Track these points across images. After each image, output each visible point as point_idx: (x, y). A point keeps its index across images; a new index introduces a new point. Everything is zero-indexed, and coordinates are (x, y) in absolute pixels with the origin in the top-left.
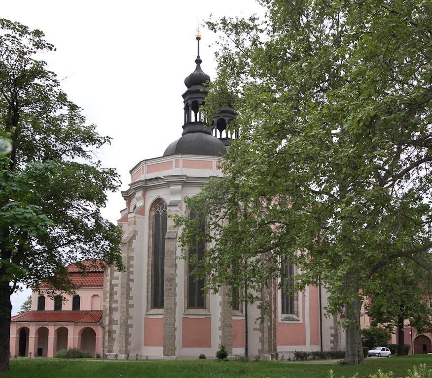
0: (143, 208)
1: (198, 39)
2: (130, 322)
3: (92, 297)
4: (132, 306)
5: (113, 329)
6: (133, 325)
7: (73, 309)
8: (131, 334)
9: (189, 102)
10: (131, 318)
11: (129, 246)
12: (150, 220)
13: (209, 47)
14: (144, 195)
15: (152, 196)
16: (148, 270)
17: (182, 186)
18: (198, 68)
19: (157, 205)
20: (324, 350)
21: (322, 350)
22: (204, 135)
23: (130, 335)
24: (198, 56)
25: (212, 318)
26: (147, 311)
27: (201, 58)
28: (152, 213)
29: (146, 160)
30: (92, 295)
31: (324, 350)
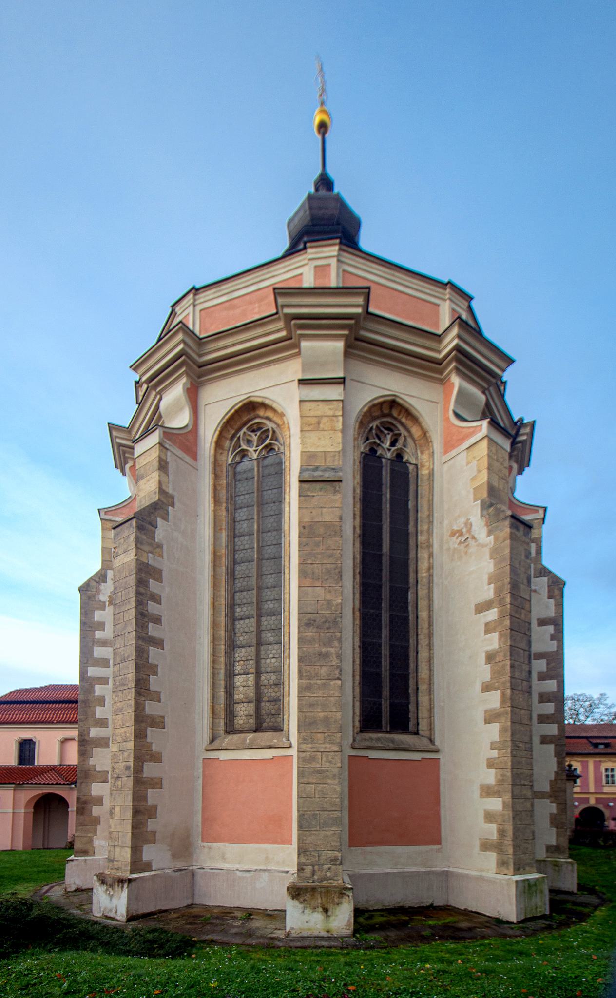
0: (194, 430)
2: (150, 770)
4: (158, 722)
5: (93, 793)
6: (481, 796)
8: (155, 807)
10: (156, 758)
19: (241, 433)
20: (236, 705)
21: (236, 703)
23: (152, 812)
25: (442, 761)
26: (212, 741)
27: (332, 173)
28: (224, 458)
29: (195, 291)
30: (60, 738)
31: (236, 705)
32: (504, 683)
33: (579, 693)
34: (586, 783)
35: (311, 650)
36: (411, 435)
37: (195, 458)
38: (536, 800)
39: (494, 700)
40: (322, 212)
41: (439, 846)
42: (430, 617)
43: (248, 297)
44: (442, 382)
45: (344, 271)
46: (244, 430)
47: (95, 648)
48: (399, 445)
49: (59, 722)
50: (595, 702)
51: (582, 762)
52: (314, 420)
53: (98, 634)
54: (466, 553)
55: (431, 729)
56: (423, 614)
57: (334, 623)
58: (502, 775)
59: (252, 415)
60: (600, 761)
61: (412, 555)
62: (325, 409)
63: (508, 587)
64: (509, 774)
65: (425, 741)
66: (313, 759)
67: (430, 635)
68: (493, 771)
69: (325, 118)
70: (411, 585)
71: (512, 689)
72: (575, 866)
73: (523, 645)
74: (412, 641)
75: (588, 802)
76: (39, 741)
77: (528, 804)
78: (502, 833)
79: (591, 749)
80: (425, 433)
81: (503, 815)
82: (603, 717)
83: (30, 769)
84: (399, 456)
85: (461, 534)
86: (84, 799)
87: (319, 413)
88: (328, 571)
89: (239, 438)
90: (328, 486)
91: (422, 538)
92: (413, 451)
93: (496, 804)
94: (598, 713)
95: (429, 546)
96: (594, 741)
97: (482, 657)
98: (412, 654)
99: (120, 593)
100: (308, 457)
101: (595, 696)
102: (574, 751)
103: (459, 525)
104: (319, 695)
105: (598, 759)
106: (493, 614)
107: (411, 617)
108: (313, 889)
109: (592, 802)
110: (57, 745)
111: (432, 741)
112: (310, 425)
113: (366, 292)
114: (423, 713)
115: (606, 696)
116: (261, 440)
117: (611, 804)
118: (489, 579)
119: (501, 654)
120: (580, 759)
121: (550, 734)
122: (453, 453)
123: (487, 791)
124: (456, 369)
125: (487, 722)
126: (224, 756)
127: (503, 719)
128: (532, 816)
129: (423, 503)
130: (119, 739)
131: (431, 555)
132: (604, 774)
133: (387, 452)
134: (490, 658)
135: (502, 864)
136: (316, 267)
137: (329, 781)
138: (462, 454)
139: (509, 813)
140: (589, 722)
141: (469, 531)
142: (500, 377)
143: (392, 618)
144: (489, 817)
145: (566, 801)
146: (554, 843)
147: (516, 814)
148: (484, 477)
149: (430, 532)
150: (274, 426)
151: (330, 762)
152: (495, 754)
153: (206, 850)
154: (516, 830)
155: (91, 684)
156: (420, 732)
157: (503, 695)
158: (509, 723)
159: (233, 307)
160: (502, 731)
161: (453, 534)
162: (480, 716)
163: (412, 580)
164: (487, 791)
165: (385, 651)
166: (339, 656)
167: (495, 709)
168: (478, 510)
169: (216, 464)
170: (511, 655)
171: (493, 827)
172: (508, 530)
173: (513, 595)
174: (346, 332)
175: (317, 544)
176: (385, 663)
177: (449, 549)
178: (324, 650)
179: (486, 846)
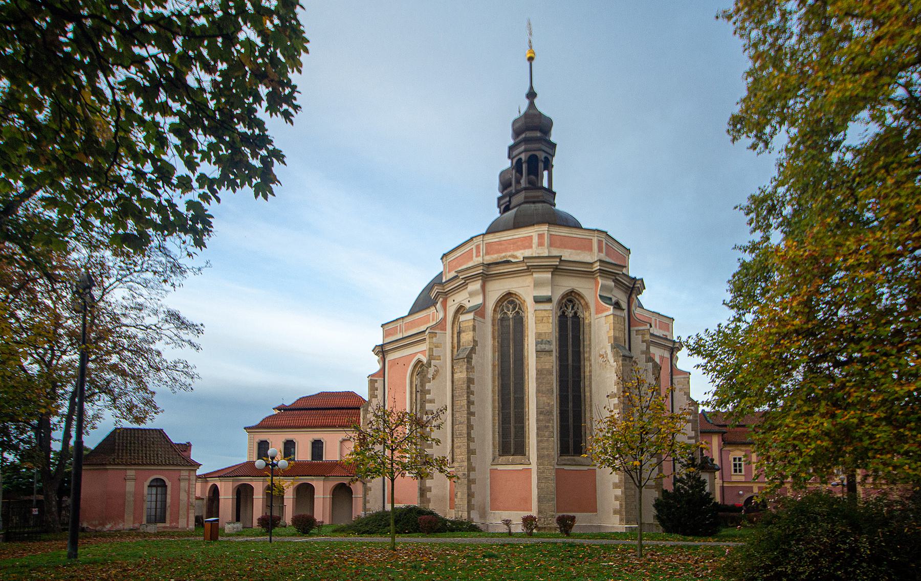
1: (531, 59)
5: (427, 485)
7: (312, 459)
11: (468, 362)
12: (493, 325)
14: (483, 287)
15: (497, 289)
16: (493, 401)
17: (552, 274)
18: (532, 105)
24: (531, 87)
26: (493, 460)
27: (536, 90)
30: (341, 439)
37: (484, 318)
42: (591, 396)
44: (595, 279)
48: (575, 308)
49: (340, 426)
53: (428, 397)
56: (588, 394)
57: (551, 413)
62: (545, 314)
66: (543, 472)
67: (591, 406)
69: (532, 55)
74: (583, 408)
75: (752, 491)
78: (621, 505)
80: (587, 304)
83: (318, 465)
84: (576, 313)
88: (548, 390)
90: (547, 353)
91: (586, 355)
93: (619, 492)
95: (590, 360)
98: (583, 415)
100: (538, 335)
104: (545, 444)
107: (582, 395)
108: (545, 528)
110: (338, 444)
112: (539, 321)
116: (514, 309)
120: (743, 448)
122: (599, 316)
126: (500, 468)
129: (587, 337)
130: (459, 461)
132: (732, 463)
133: (570, 313)
135: (621, 520)
141: (607, 357)
143: (574, 396)
148: (612, 333)
149: (590, 352)
154: (627, 504)
161: (600, 356)
163: (582, 377)
165: (571, 415)
166: (553, 427)
168: (610, 348)
169: (493, 320)
175: (543, 379)
176: (571, 421)
179: (615, 512)
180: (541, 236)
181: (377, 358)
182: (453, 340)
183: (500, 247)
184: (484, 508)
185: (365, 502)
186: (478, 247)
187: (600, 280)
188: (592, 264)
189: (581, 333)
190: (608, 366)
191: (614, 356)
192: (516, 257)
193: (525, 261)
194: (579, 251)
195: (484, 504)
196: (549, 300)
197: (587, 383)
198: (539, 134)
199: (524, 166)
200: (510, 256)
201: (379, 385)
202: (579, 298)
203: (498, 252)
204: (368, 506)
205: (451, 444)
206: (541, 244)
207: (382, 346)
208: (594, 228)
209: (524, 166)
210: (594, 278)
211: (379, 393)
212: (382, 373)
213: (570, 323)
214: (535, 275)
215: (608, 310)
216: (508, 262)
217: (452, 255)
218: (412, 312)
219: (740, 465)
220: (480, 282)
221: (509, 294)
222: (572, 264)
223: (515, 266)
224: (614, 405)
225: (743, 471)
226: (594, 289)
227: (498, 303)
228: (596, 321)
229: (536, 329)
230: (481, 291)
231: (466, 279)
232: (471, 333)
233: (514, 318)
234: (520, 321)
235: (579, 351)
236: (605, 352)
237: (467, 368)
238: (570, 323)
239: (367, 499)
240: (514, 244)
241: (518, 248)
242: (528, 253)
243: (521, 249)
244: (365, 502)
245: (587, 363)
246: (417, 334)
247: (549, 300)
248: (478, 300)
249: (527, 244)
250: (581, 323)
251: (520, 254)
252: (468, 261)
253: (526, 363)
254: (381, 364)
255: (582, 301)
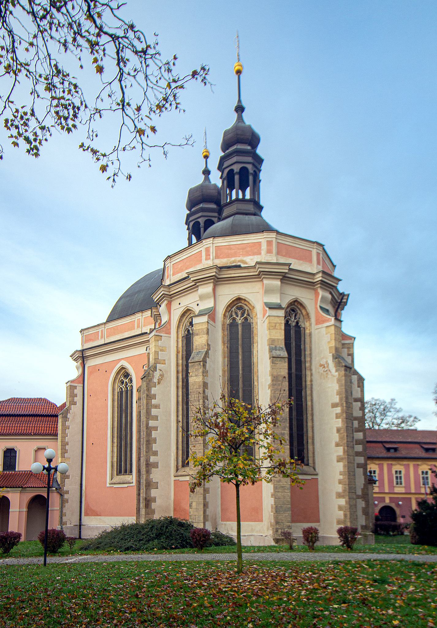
1: (239, 72)
3: (36, 451)
5: (152, 495)
6: (337, 498)
7: (4, 470)
9: (233, 167)
13: (184, 111)
14: (214, 290)
18: (240, 119)
19: (233, 309)
22: (253, 217)
24: (239, 101)
25: (319, 479)
27: (244, 104)
30: (35, 448)
32: (344, 444)
33: (376, 398)
34: (382, 486)
35: (278, 432)
36: (302, 313)
38: (357, 500)
39: (340, 451)
40: (242, 137)
41: (319, 524)
42: (312, 406)
43: (237, 246)
44: (315, 290)
45: (278, 242)
46: (235, 307)
47: (152, 409)
48: (297, 317)
49: (35, 435)
50: (388, 406)
51: (379, 464)
52: (274, 325)
53: (154, 402)
54: (327, 377)
55: (314, 463)
56: (309, 403)
58: (345, 488)
59: (239, 302)
60: (391, 464)
61: (303, 372)
63: (344, 399)
64: (347, 487)
65: (312, 469)
67: (312, 415)
68: (341, 485)
70: (303, 388)
71: (347, 447)
72: (374, 536)
73: (350, 425)
75: (384, 501)
76: (19, 450)
77: (354, 502)
78: (345, 515)
79: (384, 454)
80: (308, 314)
81: (346, 507)
82: (394, 420)
84: (297, 323)
85: (324, 367)
86: (148, 498)
87: (275, 322)
89: (232, 311)
90: (282, 359)
92: (303, 320)
93: (342, 502)
94: (390, 416)
95: (311, 370)
96: (388, 446)
97: (335, 430)
99: (193, 396)
101: (388, 400)
102: (373, 455)
103: (323, 362)
105: (390, 462)
106: (338, 410)
107: (304, 404)
109: (387, 501)
110: (33, 453)
111: (314, 469)
113: (289, 265)
114: (310, 455)
115: (395, 401)
116: (243, 315)
117: (400, 503)
118: (337, 392)
119: (343, 429)
120: (377, 462)
121: (360, 462)
122: (320, 326)
123: (339, 496)
124: (320, 287)
125: (338, 461)
127: (344, 461)
128: (356, 507)
129: (307, 346)
131: (311, 375)
132: (395, 476)
134: (338, 430)
136: (267, 241)
137: (286, 491)
138: (323, 329)
139: (348, 506)
140: (384, 426)
141: (328, 366)
142: (336, 287)
144: (340, 508)
145: (368, 500)
146: (364, 524)
147: (351, 506)
148: (333, 344)
150: (248, 309)
151: (286, 482)
152: (341, 477)
153: (223, 526)
155: (150, 430)
156: (310, 464)
157: (344, 449)
158: (346, 463)
159: (231, 249)
160: (344, 466)
161: (321, 365)
162: (335, 459)
164: (339, 496)
167: (340, 456)
169: (223, 325)
170: (347, 431)
171: (342, 513)
172: (343, 372)
173: (347, 402)
174: (281, 277)
177: (319, 372)
178: (283, 432)
180: (269, 243)
181: (75, 363)
182: (177, 344)
183: (230, 251)
184: (216, 519)
185: (62, 515)
186: (207, 250)
187: (321, 292)
188: (314, 275)
189: (302, 343)
190: (329, 376)
191: (336, 366)
192: (245, 263)
193: (257, 266)
194: (301, 262)
195: (216, 516)
196: (278, 307)
197: (308, 392)
198: (249, 148)
199: (237, 177)
200: (239, 261)
201: (78, 391)
202: (301, 308)
203: (228, 256)
204: (65, 519)
205: (175, 451)
206: (269, 251)
207: (83, 351)
208: (314, 241)
209: (237, 177)
210: (314, 289)
211: (78, 399)
212: (81, 379)
213: (293, 332)
214: (266, 282)
215: (328, 320)
216: (239, 266)
217: (177, 257)
218: (111, 319)
219: (401, 477)
220: (212, 285)
221: (239, 299)
222: (297, 274)
223: (246, 271)
224: (336, 414)
225: (403, 482)
226: (314, 301)
227: (227, 308)
228: (317, 331)
229: (270, 335)
230: (212, 294)
231: (197, 281)
232: (205, 337)
233: (243, 324)
234: (248, 327)
235: (301, 361)
236: (327, 362)
237: (203, 372)
238: (293, 332)
239: (64, 511)
240: (243, 249)
241: (248, 254)
242: (257, 258)
243: (250, 255)
244: (62, 515)
245: (308, 373)
246: (123, 340)
247: (278, 307)
248: (209, 304)
249: (256, 251)
250: (302, 332)
251: (251, 260)
252: (196, 264)
253: (255, 370)
254: (81, 370)
255: (303, 311)
